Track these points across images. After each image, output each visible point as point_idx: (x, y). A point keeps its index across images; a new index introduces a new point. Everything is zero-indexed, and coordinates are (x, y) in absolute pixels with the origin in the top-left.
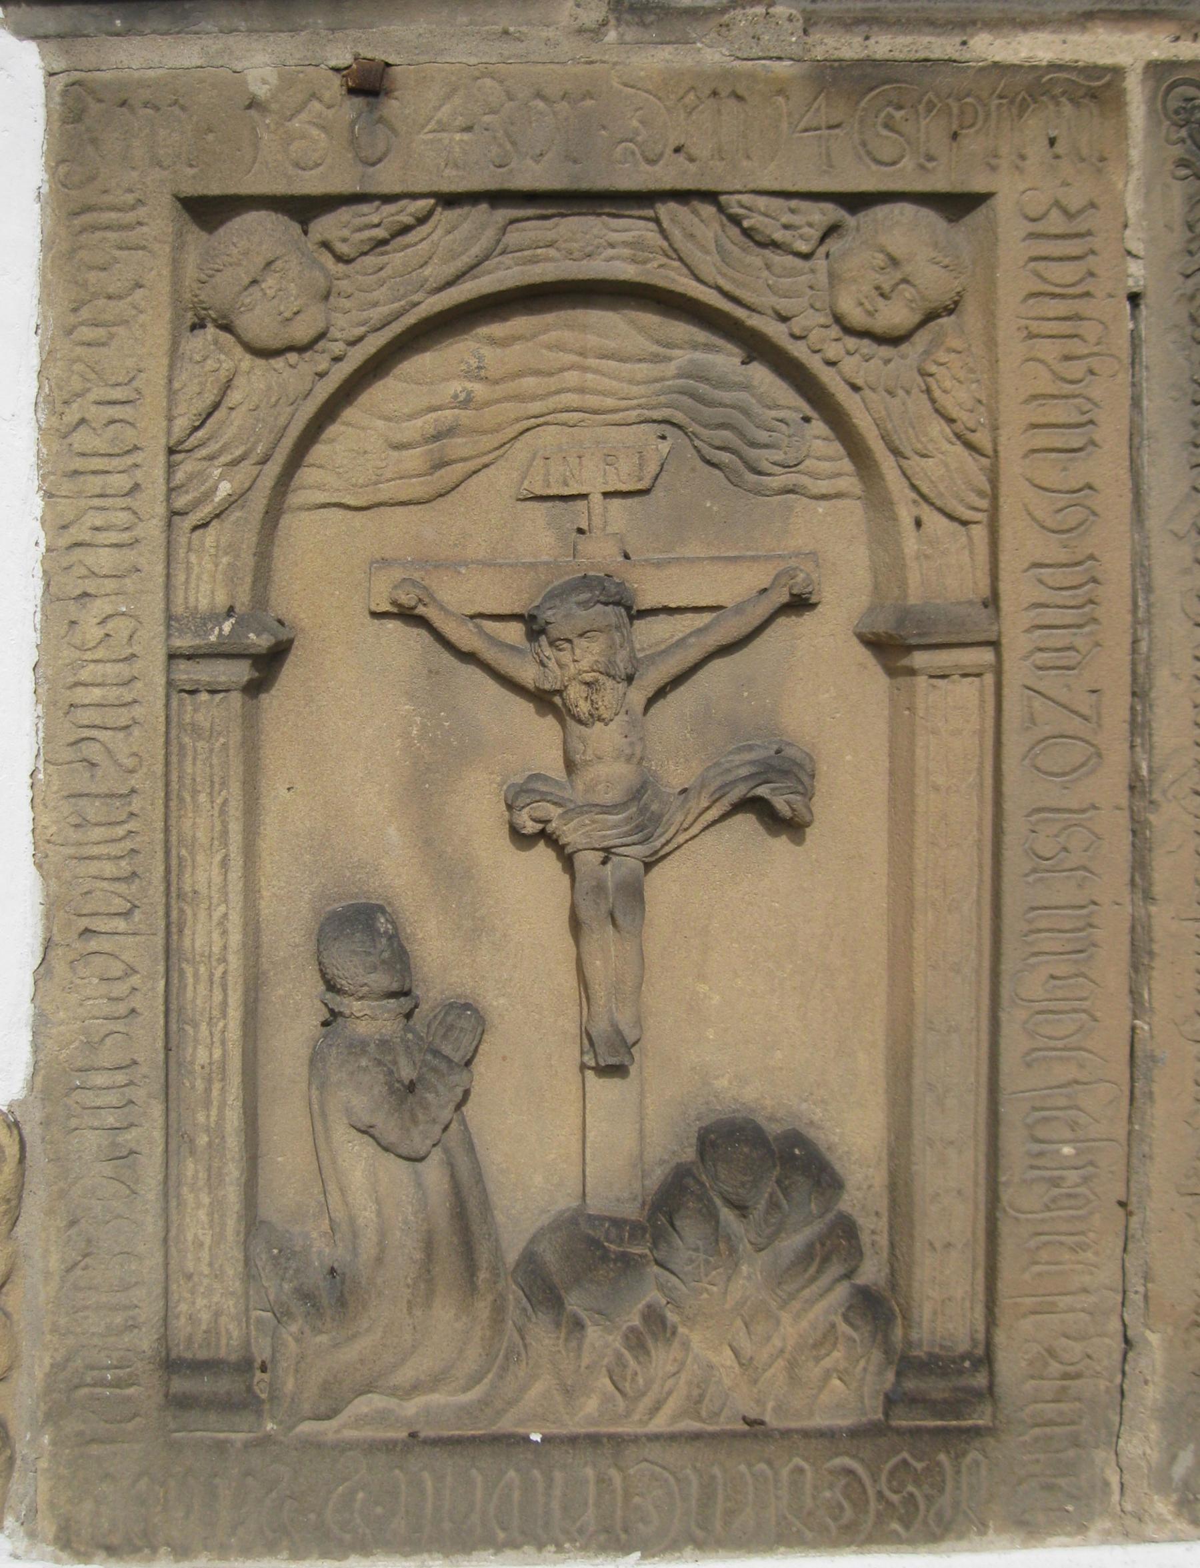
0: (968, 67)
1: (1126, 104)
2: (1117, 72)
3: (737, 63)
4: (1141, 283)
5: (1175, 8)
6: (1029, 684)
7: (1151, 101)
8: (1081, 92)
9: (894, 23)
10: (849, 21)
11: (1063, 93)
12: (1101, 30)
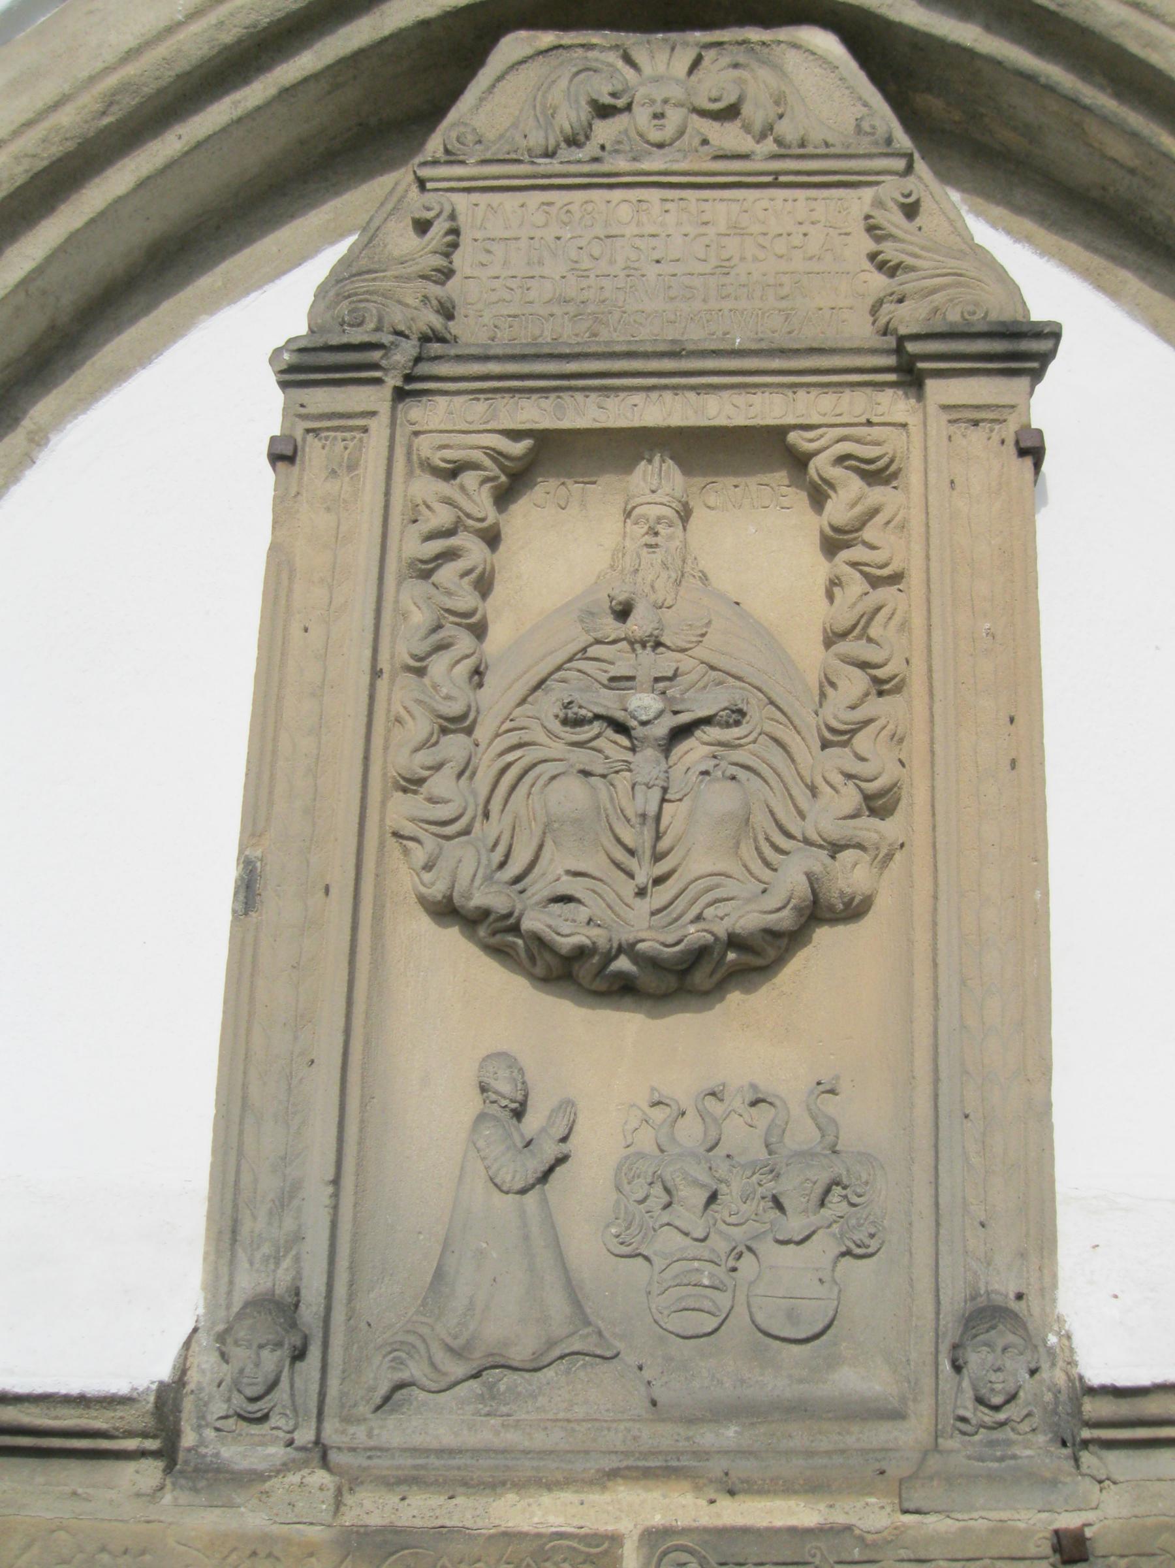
0: (479, 1535)
2: (615, 1539)
3: (275, 1528)
5: (695, 1464)
8: (580, 1559)
9: (432, 1484)
10: (392, 1480)
11: (564, 1560)
12: (622, 1488)
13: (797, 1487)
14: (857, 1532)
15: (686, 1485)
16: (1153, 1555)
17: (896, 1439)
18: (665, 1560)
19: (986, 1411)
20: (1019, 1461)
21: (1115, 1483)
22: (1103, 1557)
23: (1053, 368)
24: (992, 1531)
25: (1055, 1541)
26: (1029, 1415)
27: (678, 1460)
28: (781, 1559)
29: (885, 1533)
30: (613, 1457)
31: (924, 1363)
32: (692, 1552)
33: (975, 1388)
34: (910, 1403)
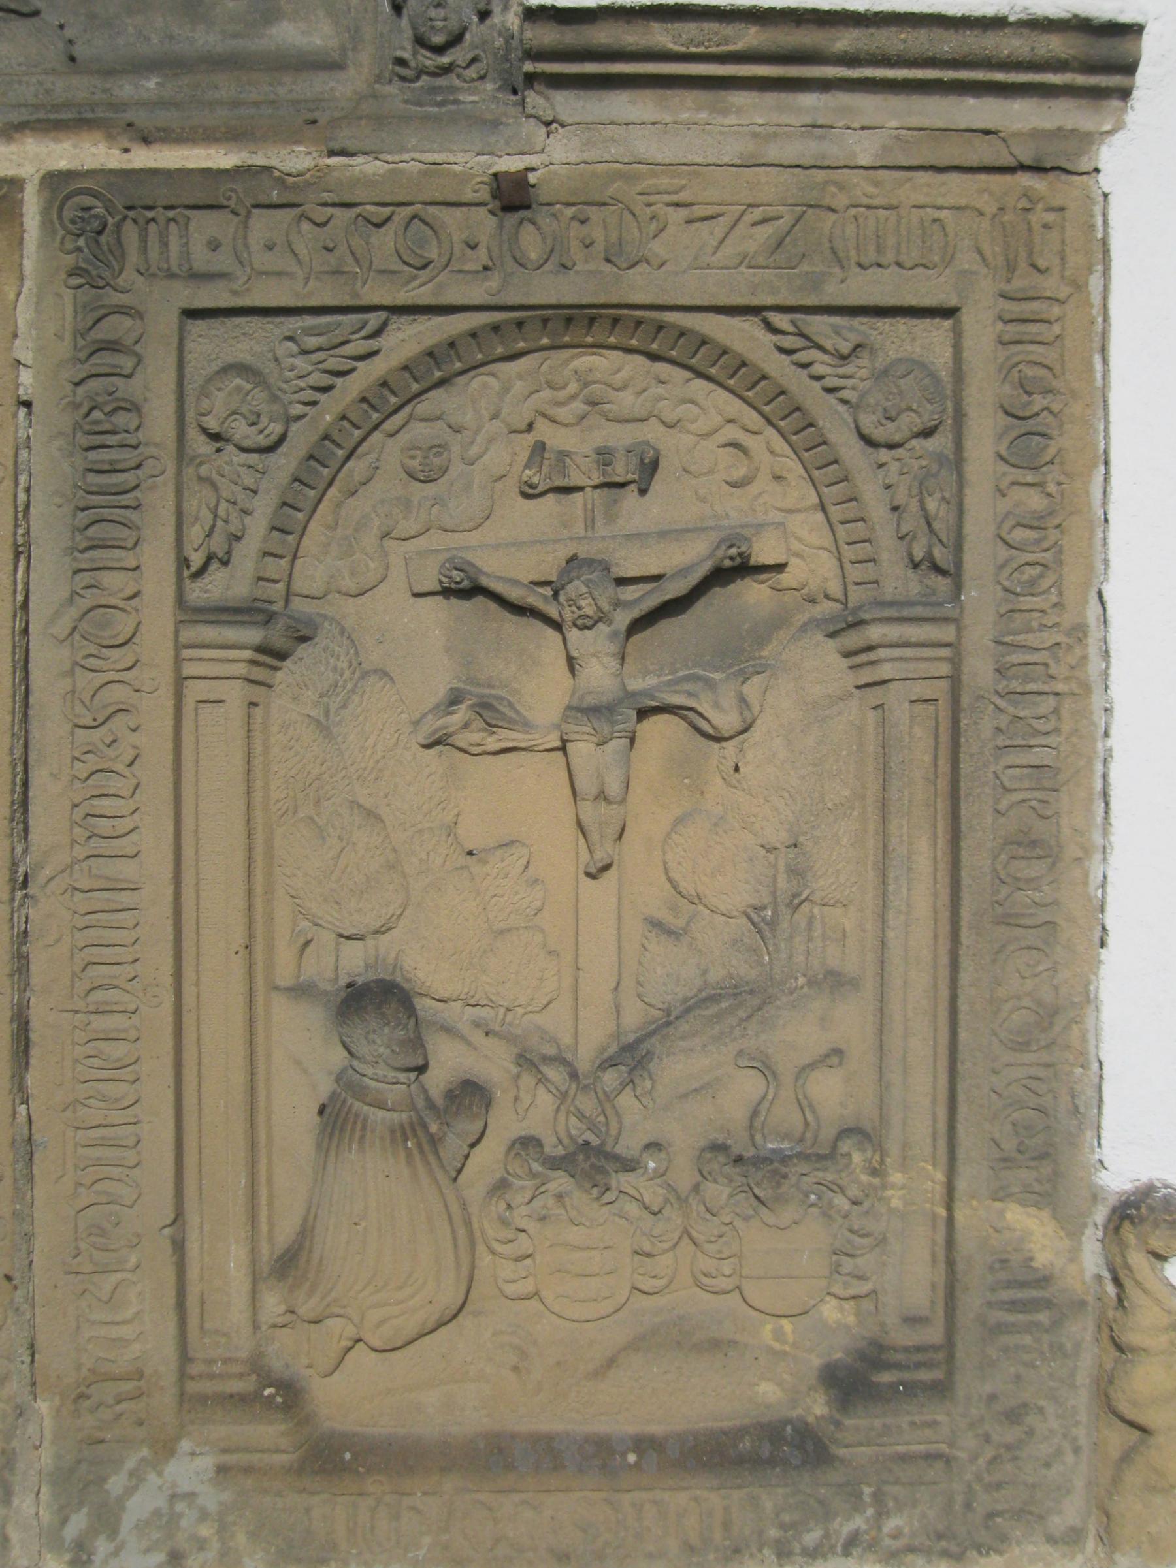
1: (22, 215)
4: (30, 391)
5: (111, 115)
6: (376, 359)
7: (45, 212)
12: (30, 140)
13: (218, 135)
14: (277, 174)
15: (98, 135)
16: (605, 204)
17: (332, 89)
18: (69, 204)
19: (428, 54)
20: (462, 107)
21: (563, 126)
22: (548, 204)
23: (1136, 94)
24: (424, 174)
25: (495, 186)
26: (474, 60)
27: (93, 111)
28: (192, 202)
29: (308, 176)
30: (23, 110)
31: (366, 11)
32: (95, 195)
33: (414, 28)
34: (350, 53)
